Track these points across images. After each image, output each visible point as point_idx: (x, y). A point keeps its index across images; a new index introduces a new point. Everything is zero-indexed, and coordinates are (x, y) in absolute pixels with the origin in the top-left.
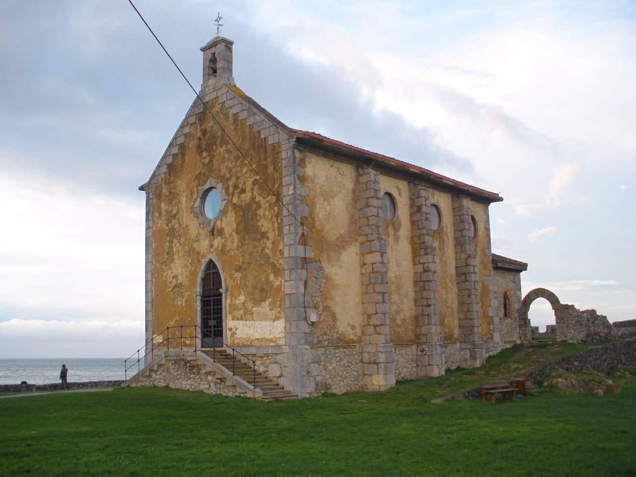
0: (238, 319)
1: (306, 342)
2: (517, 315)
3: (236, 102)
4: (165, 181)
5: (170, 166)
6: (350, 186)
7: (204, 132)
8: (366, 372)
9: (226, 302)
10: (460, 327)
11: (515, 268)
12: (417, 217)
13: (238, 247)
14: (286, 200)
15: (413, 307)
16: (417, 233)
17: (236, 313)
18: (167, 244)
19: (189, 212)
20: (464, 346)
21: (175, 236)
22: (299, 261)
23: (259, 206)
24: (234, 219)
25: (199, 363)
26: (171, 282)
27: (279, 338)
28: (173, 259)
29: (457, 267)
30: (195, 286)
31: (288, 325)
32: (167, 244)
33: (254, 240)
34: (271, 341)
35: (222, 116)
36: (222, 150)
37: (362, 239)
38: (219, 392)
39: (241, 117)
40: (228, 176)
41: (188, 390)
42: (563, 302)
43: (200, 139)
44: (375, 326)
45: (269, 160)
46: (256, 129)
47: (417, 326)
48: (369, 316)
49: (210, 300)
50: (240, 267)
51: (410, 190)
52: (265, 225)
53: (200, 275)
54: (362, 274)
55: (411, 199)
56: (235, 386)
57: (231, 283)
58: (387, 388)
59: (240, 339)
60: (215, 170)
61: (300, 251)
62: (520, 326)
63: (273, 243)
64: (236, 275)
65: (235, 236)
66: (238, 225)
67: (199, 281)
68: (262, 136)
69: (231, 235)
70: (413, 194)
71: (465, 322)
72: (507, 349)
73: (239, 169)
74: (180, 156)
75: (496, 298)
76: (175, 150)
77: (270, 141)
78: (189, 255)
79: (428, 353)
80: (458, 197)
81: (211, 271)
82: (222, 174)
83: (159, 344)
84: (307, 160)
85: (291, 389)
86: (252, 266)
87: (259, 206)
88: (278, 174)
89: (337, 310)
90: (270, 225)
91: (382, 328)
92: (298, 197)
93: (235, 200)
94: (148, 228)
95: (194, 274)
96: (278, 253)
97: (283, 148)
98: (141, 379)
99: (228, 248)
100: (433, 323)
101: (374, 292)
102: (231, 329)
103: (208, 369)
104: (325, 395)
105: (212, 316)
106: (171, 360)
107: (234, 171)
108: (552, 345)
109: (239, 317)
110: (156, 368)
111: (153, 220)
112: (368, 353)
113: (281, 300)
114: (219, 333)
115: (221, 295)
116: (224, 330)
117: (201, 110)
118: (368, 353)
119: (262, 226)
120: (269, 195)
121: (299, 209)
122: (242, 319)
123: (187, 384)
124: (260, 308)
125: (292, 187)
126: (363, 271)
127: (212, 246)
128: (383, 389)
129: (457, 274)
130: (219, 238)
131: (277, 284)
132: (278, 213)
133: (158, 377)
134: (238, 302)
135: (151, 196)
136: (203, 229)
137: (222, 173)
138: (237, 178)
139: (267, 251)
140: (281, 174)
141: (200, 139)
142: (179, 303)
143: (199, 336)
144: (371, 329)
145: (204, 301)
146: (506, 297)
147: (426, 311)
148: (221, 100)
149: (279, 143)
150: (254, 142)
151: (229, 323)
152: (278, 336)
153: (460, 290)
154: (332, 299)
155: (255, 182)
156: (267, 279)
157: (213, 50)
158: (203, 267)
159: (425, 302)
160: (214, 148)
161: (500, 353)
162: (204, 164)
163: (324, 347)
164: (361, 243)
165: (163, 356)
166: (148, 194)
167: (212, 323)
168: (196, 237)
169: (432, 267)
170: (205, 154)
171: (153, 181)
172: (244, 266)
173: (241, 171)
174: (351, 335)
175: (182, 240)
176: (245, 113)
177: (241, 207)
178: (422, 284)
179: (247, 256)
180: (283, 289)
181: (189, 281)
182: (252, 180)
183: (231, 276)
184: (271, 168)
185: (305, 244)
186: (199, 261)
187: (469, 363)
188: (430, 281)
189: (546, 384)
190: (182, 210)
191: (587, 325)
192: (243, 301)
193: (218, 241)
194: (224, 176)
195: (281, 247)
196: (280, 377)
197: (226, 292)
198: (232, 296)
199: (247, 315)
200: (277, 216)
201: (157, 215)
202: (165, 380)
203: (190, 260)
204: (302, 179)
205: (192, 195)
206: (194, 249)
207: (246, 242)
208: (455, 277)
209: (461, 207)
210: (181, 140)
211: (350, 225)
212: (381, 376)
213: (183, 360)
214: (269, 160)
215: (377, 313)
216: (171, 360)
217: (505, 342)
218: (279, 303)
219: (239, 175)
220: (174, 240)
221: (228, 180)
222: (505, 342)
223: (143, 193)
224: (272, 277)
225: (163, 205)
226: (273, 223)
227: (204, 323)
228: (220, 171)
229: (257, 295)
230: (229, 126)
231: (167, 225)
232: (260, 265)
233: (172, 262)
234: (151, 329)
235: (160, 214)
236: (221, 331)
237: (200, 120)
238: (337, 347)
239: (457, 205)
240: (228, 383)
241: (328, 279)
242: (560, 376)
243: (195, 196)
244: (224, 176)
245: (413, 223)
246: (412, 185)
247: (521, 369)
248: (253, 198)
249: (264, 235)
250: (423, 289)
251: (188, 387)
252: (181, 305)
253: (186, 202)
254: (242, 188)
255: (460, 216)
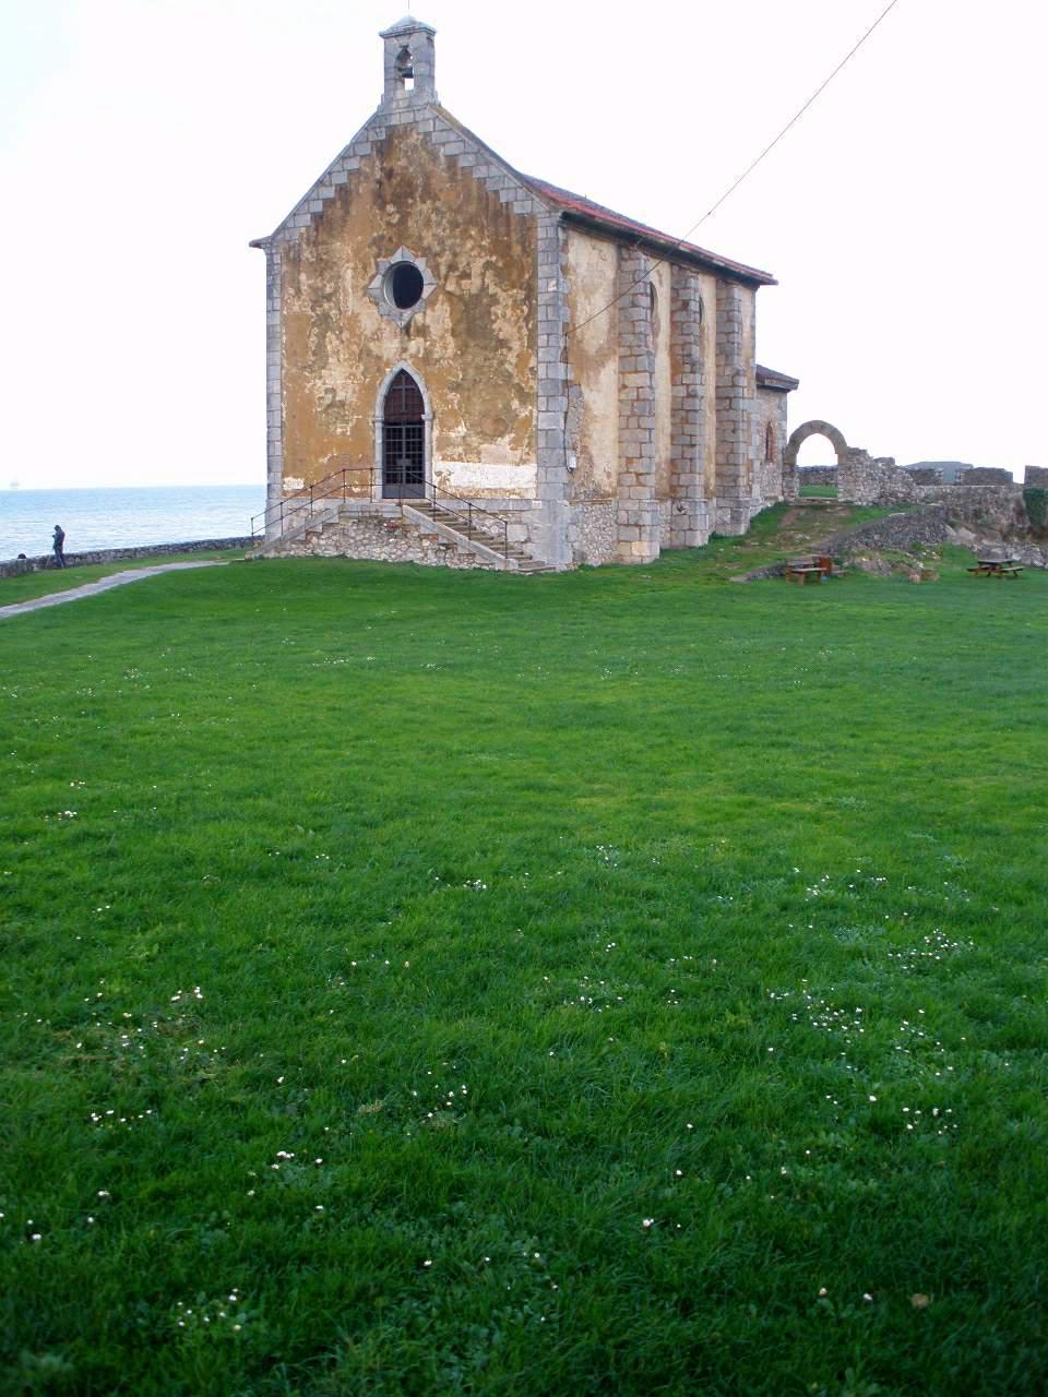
0: (454, 460)
1: (565, 497)
2: (780, 457)
3: (453, 137)
4: (308, 239)
5: (318, 218)
6: (610, 274)
7: (390, 174)
8: (621, 538)
9: (431, 434)
10: (719, 475)
11: (776, 386)
12: (680, 317)
13: (456, 354)
14: (542, 299)
15: (669, 446)
16: (680, 340)
17: (449, 451)
18: (313, 338)
19: (360, 293)
20: (722, 503)
21: (328, 328)
22: (560, 385)
23: (494, 300)
24: (447, 315)
25: (407, 522)
26: (320, 398)
27: (527, 489)
28: (326, 363)
29: (717, 387)
30: (373, 407)
31: (542, 472)
32: (313, 338)
33: (485, 348)
34: (512, 492)
35: (424, 153)
36: (426, 207)
37: (623, 351)
38: (442, 563)
39: (463, 162)
40: (437, 249)
41: (385, 560)
42: (851, 443)
43: (380, 182)
44: (638, 475)
45: (514, 237)
46: (490, 186)
47: (673, 473)
48: (629, 460)
49: (400, 430)
50: (459, 385)
51: (672, 274)
52: (504, 327)
53: (382, 391)
54: (620, 401)
55: (673, 289)
56: (474, 555)
57: (441, 408)
58: (653, 559)
59: (456, 487)
60: (410, 236)
61: (561, 372)
62: (784, 475)
63: (518, 356)
64: (451, 396)
65: (450, 339)
66: (456, 323)
67: (380, 400)
68: (503, 200)
69: (442, 337)
70: (677, 283)
71: (726, 468)
72: (768, 508)
73: (458, 241)
74: (339, 204)
75: (758, 431)
76: (330, 193)
77: (517, 209)
78: (360, 359)
79: (689, 513)
80: (727, 283)
81: (403, 387)
82: (425, 243)
83: (297, 493)
84: (570, 242)
85: (544, 559)
86: (481, 386)
87: (494, 300)
88: (530, 260)
89: (594, 451)
90: (515, 330)
91: (648, 477)
92: (561, 296)
93: (451, 287)
94: (270, 311)
95: (368, 390)
96: (527, 371)
97: (540, 222)
98: (288, 545)
99: (436, 356)
100: (698, 470)
101: (639, 427)
102: (439, 474)
103: (423, 531)
104: (582, 567)
105: (404, 453)
106: (350, 518)
107: (449, 242)
108: (831, 507)
109: (456, 457)
110: (320, 529)
111: (282, 299)
112: (627, 511)
113: (530, 437)
114: (416, 475)
115: (422, 422)
116: (427, 475)
117: (383, 137)
118: (627, 511)
119: (500, 330)
120: (513, 287)
121: (561, 312)
122: (461, 460)
123: (381, 551)
124: (493, 446)
125: (554, 282)
126: (623, 397)
127: (405, 350)
128: (647, 561)
129: (717, 398)
130: (421, 340)
131: (523, 414)
132: (528, 315)
133: (322, 542)
134: (453, 435)
135: (277, 259)
136: (389, 322)
137: (425, 243)
138: (455, 255)
139: (507, 366)
140: (535, 260)
141: (380, 182)
142: (339, 430)
143: (379, 481)
144: (631, 479)
145: (388, 430)
146: (769, 431)
147: (689, 453)
148: (422, 128)
149: (533, 217)
150: (487, 205)
151: (436, 466)
152: (525, 486)
153: (719, 421)
154: (590, 437)
155: (488, 265)
156: (507, 407)
157: (404, 41)
158: (388, 379)
159: (687, 440)
160: (410, 201)
161: (760, 514)
162: (389, 224)
163: (582, 502)
164: (621, 357)
165: (335, 512)
166: (270, 257)
167: (404, 462)
168: (374, 333)
169: (700, 390)
170: (390, 208)
171: (280, 237)
172: (466, 385)
173: (462, 245)
174: (607, 485)
175: (345, 335)
176: (471, 158)
177: (461, 298)
178: (684, 414)
179: (471, 372)
180: (534, 422)
181: (358, 398)
182: (483, 261)
183: (442, 397)
184: (517, 250)
185: (566, 361)
186: (380, 370)
187: (729, 528)
188: (695, 411)
189: (846, 564)
190: (345, 290)
191: (881, 480)
192: (462, 434)
193: (416, 345)
194: (429, 248)
195: (532, 363)
196: (526, 542)
197: (432, 420)
198: (442, 425)
199: (470, 453)
200: (527, 319)
201: (292, 291)
202: (337, 548)
203: (362, 368)
204: (565, 270)
205: (365, 268)
206: (369, 353)
207: (470, 350)
208: (714, 401)
209: (730, 299)
210: (342, 179)
211: (609, 332)
212: (646, 544)
213: (376, 517)
214: (514, 237)
215: (641, 457)
216: (350, 518)
217: (766, 498)
218: (526, 441)
219: (458, 250)
220: (329, 334)
221: (438, 255)
222: (766, 498)
223: (260, 255)
224: (515, 404)
225: (303, 277)
226: (520, 328)
227: (388, 462)
228: (420, 238)
229: (488, 427)
230: (440, 171)
231: (313, 309)
232: (496, 386)
233: (324, 368)
234: (278, 468)
235: (298, 291)
236: (422, 475)
237: (380, 151)
238: (594, 503)
239: (724, 295)
240: (460, 550)
241: (586, 408)
242: (862, 554)
243: (372, 271)
244: (429, 248)
245: (673, 324)
246: (676, 268)
247: (809, 541)
248: (484, 288)
249: (503, 343)
250: (685, 421)
251: (383, 556)
252: (343, 434)
253: (353, 277)
254: (464, 272)
255: (728, 312)
